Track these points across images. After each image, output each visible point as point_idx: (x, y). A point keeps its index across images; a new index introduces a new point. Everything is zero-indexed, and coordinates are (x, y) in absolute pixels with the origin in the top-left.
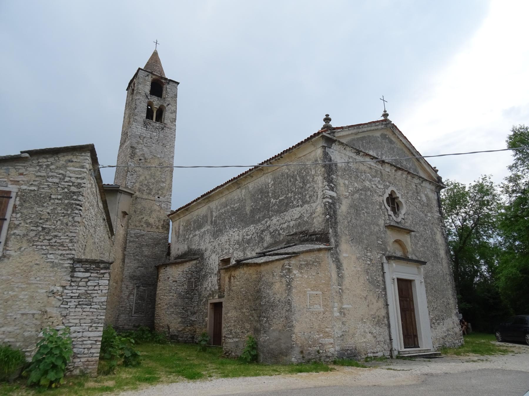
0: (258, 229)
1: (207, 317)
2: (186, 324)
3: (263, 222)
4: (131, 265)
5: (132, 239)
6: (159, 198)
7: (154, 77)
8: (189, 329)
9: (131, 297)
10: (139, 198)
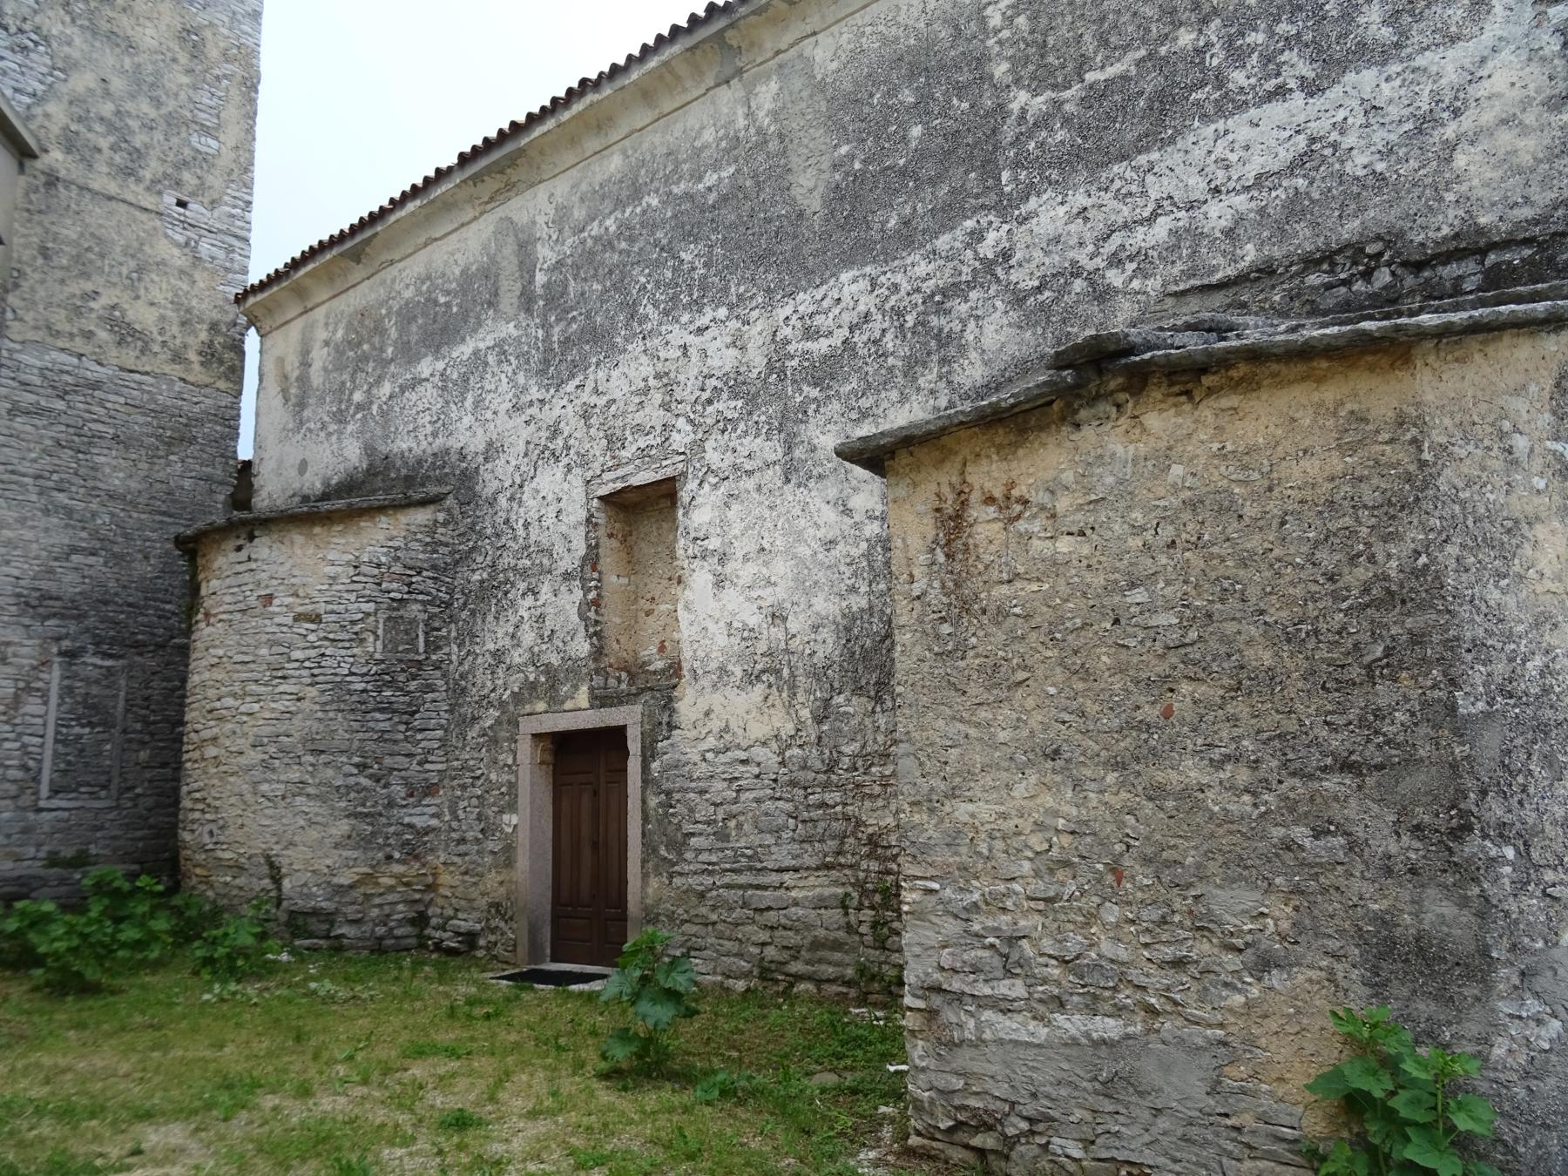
0: (905, 287)
1: (512, 807)
2: (380, 847)
5: (31, 398)
6: (182, 204)
8: (398, 877)
9: (29, 709)
10: (68, 184)
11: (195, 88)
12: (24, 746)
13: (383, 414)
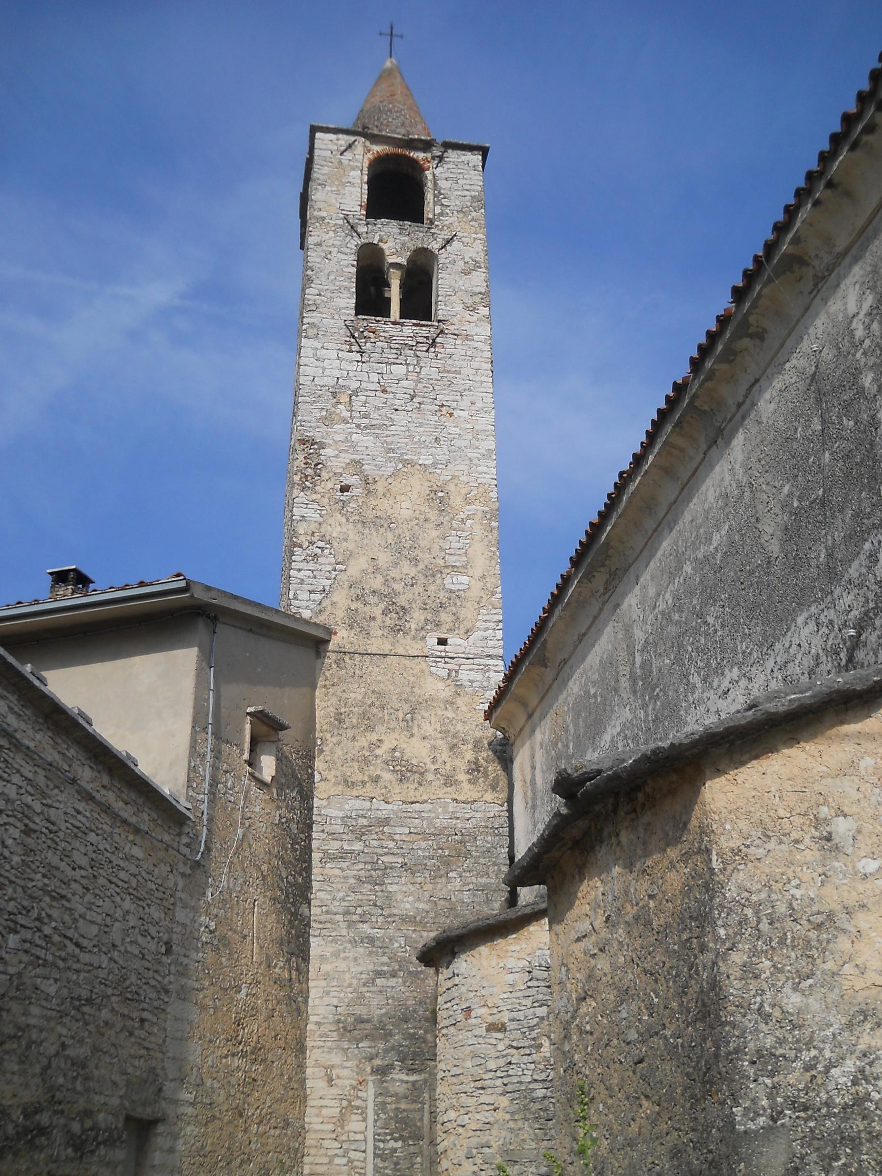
3: (854, 571)
4: (342, 966)
5: (336, 845)
6: (442, 642)
7: (378, 149)
12: (351, 1161)
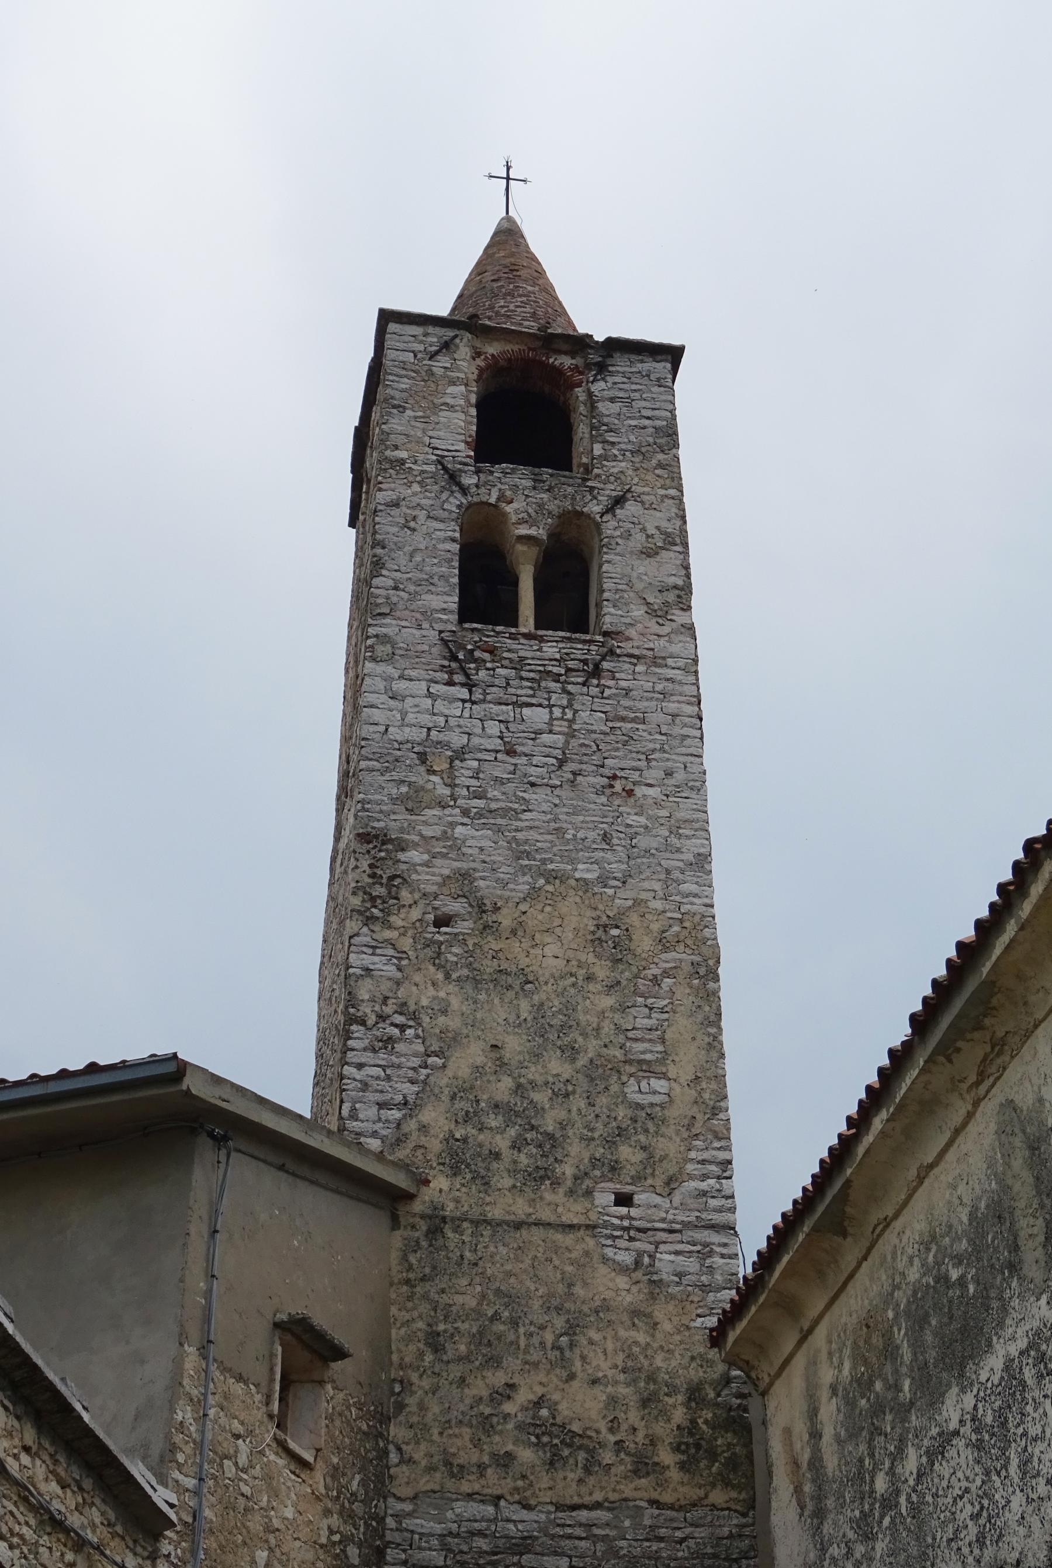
6: (624, 1200)
10: (457, 1223)
11: (623, 1009)
13: (915, 1510)
